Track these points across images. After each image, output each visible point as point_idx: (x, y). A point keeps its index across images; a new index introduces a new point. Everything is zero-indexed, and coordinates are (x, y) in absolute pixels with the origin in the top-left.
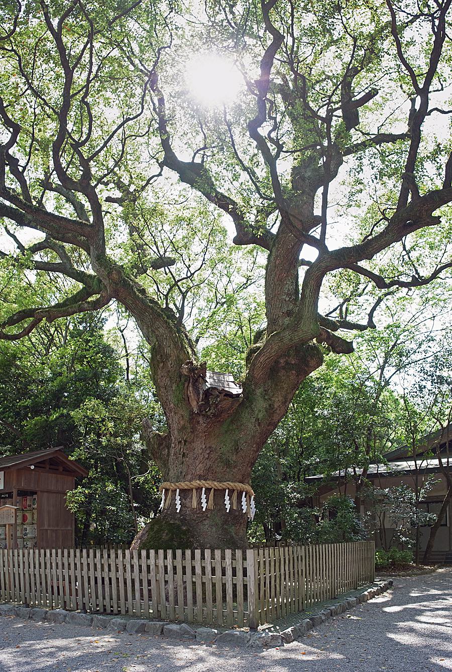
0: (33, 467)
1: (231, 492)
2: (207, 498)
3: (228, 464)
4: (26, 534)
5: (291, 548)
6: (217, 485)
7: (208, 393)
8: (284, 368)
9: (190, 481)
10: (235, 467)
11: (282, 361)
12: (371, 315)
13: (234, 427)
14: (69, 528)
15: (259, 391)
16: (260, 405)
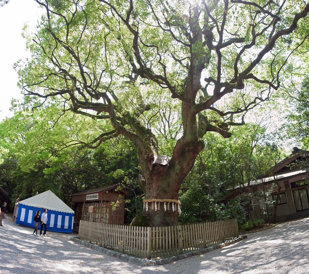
0: (107, 192)
1: (167, 203)
2: (157, 206)
3: (165, 192)
4: (106, 217)
5: (169, 227)
6: (160, 200)
7: (155, 165)
8: (187, 152)
9: (151, 199)
10: (168, 193)
11: (187, 149)
12: (243, 119)
13: (168, 177)
14: (122, 216)
15: (177, 162)
16: (178, 167)
